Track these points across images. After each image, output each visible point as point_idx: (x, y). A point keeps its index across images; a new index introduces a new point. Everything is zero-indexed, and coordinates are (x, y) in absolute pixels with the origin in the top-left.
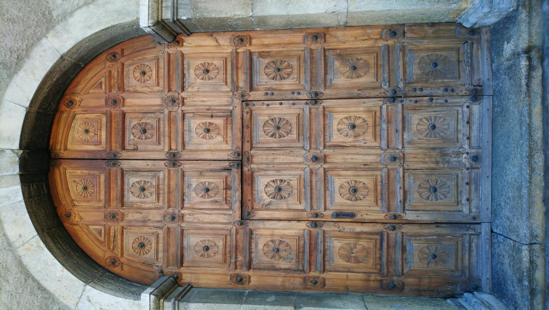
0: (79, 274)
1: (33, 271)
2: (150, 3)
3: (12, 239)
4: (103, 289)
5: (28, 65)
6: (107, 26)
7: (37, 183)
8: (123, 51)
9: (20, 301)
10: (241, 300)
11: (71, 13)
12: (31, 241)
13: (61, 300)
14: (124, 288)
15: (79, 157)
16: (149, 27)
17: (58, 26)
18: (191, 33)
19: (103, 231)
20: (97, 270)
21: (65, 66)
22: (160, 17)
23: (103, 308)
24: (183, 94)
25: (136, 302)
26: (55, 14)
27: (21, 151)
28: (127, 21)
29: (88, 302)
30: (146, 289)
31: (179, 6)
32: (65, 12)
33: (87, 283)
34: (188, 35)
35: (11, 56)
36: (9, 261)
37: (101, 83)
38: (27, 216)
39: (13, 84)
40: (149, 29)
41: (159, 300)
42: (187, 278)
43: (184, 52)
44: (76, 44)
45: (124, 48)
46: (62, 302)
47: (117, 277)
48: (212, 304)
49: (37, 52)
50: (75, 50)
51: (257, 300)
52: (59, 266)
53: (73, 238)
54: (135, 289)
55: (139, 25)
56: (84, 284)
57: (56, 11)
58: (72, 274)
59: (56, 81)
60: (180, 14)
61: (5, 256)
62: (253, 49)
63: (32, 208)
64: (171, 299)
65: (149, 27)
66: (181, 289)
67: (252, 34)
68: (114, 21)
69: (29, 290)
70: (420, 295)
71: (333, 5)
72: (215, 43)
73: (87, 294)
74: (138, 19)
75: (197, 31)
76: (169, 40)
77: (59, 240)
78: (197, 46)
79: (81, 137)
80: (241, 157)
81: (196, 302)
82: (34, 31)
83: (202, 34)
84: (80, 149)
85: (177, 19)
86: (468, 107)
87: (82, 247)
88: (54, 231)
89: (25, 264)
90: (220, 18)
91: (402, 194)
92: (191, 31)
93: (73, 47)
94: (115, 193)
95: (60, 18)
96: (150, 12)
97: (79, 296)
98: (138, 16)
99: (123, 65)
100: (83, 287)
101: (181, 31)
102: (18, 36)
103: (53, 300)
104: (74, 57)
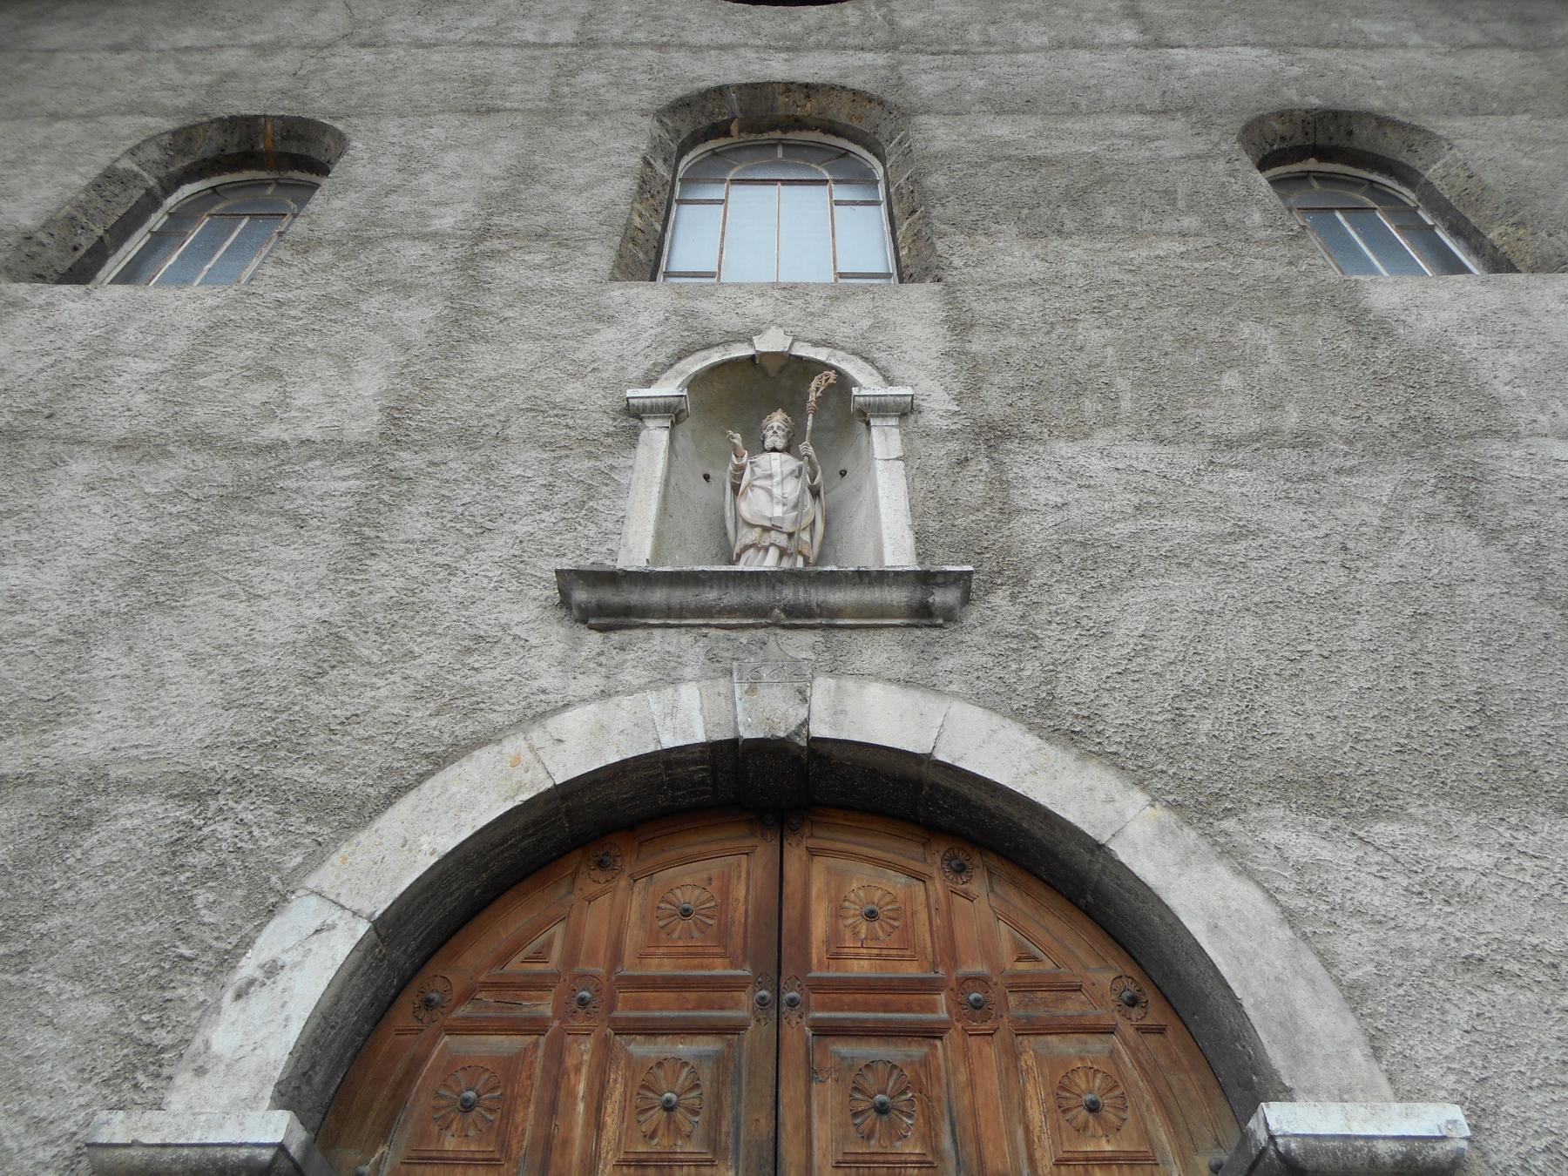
1: (451, 772)
2: (1359, 1143)
3: (553, 724)
4: (344, 974)
5: (1059, 757)
6: (1233, 985)
7: (709, 781)
8: (1161, 1031)
9: (374, 743)
11: (1245, 872)
12: (540, 767)
13: (345, 849)
14: (333, 1041)
15: (787, 889)
17: (1194, 834)
19: (539, 967)
20: (418, 949)
21: (1072, 854)
25: (269, 1091)
26: (1230, 824)
27: (803, 743)
28: (1270, 1053)
29: (317, 924)
32: (1243, 855)
35: (1077, 716)
36: (492, 716)
37: (1035, 959)
38: (614, 758)
39: (996, 720)
40: (1262, 1136)
45: (1170, 1033)
46: (337, 849)
49: (1101, 779)
52: (449, 841)
54: (318, 1079)
56: (377, 915)
57: (1240, 827)
61: (508, 707)
63: (637, 769)
68: (1256, 1006)
69: (396, 765)
74: (1286, 1094)
82: (1162, 772)
89: (476, 753)
94: (664, 1008)
95: (1222, 840)
96: (1331, 1144)
97: (342, 901)
98: (1298, 1093)
99: (1110, 1031)
102: (1136, 734)
103: (350, 826)
104: (1106, 880)
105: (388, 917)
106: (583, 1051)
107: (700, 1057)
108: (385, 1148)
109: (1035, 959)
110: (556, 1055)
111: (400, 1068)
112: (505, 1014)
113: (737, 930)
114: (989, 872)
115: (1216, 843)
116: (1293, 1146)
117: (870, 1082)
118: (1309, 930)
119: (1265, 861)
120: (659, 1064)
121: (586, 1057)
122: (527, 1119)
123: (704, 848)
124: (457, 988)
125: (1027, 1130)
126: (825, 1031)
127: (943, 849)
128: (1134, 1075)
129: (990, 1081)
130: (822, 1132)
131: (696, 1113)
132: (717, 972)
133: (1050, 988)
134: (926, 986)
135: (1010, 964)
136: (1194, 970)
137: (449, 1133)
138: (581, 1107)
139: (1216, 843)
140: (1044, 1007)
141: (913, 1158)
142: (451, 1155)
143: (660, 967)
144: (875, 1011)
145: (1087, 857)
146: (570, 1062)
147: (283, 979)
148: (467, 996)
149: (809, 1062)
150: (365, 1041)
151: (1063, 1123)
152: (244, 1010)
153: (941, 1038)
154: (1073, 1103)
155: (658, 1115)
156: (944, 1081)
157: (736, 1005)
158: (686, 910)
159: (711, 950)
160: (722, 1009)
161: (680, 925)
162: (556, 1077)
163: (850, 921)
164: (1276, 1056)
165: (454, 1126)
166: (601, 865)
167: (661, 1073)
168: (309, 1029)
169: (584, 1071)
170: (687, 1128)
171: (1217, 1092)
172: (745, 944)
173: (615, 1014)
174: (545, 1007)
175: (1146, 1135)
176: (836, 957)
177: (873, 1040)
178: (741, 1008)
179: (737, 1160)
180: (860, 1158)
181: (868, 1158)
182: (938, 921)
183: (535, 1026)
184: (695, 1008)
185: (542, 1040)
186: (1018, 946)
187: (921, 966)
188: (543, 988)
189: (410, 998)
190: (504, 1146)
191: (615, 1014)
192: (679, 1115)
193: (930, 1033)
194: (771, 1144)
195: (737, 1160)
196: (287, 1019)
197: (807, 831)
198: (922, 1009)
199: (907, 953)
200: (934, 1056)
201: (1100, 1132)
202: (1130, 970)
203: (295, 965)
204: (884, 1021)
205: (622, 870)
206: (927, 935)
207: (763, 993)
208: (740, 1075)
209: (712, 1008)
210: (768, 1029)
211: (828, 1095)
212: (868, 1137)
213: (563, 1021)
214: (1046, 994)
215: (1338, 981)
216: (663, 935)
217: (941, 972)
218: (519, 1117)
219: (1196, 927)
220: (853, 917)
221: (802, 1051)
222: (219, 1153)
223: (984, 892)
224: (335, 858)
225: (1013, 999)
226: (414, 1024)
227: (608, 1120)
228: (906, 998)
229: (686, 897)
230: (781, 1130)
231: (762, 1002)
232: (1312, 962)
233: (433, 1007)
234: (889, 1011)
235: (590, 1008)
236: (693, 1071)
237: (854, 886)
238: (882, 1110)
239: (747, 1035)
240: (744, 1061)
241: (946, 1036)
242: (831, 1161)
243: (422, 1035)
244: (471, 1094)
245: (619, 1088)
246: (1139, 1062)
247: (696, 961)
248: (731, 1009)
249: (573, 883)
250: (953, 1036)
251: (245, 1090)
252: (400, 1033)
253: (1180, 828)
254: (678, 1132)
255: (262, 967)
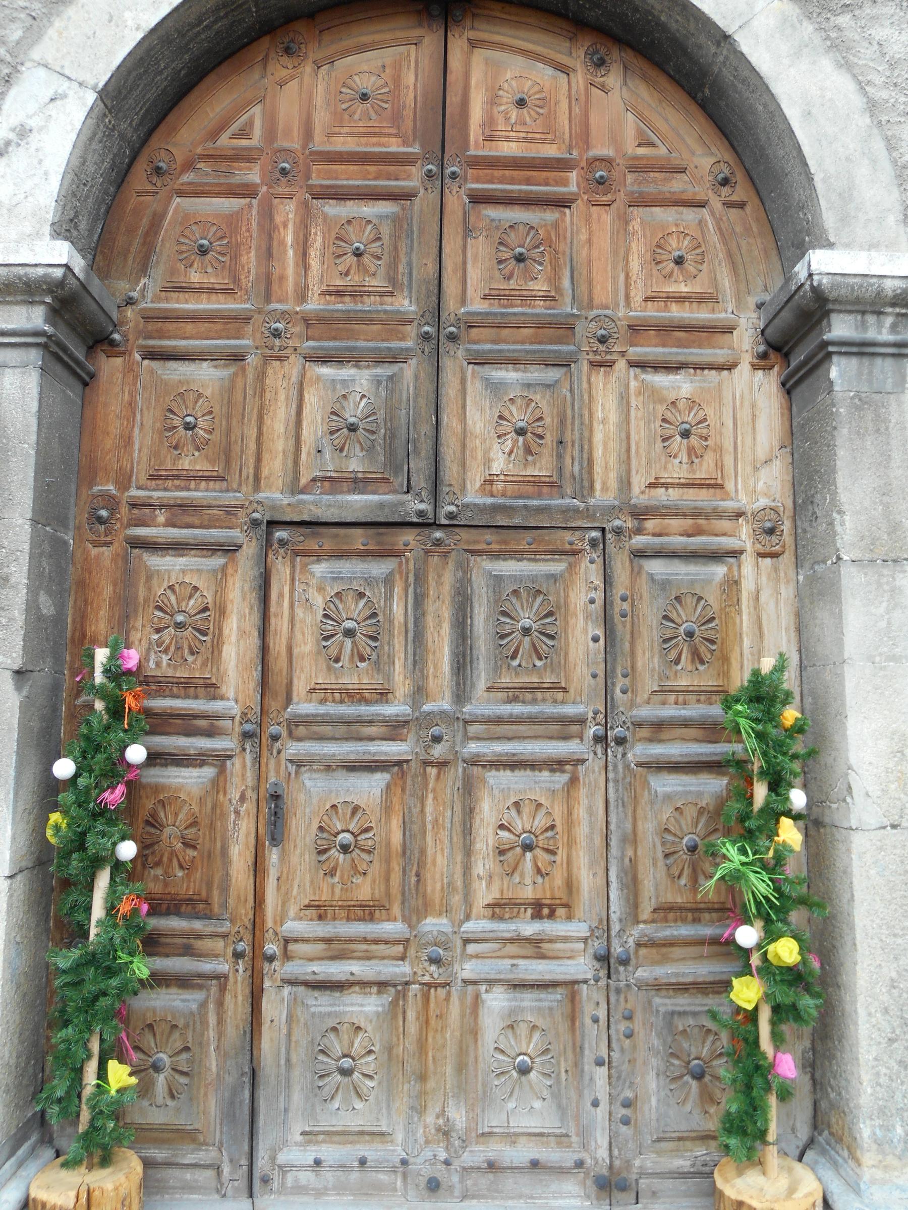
0: (129, 72)
4: (83, 138)
6: (811, 162)
8: (741, 205)
10: (43, 521)
11: (846, 65)
13: (58, 23)
14: (87, 197)
16: (810, 275)
17: (810, 28)
18: (789, 392)
19: (244, 143)
20: (140, 124)
21: (700, 47)
22: (837, 307)
23: (32, 135)
24: (621, 364)
25: (47, 229)
26: (844, 20)
29: (50, 94)
30: (84, 257)
31: (866, 361)
32: (849, 49)
33: (103, 94)
34: (783, 384)
37: (653, 145)
40: (803, 275)
41: (50, 292)
42: (110, 368)
43: (736, 371)
44: (761, 78)
45: (748, 209)
46: (51, 23)
47: (120, 176)
48: (33, 438)
50: (746, 73)
51: (44, 564)
53: (226, 63)
54: (83, 225)
55: (814, 248)
56: (101, 85)
57: (853, 23)
58: (130, 54)
59: (659, 24)
60: (844, 361)
62: (748, 563)
64: (53, 325)
65: (810, 275)
66: (80, 355)
67: (787, 558)
70: (619, 218)
71: (870, 789)
72: (761, 455)
73: (71, 93)
74: (830, 245)
75: (794, 408)
76: (768, 331)
77: (225, 22)
78: (753, 406)
79: (506, 86)
80: (444, 521)
81: (41, 394)
83: (787, 424)
84: (473, 82)
85: (829, 355)
86: (580, 1164)
87: (203, 86)
88: (249, 10)
90: (834, 471)
91: (337, 978)
92: (796, 393)
93: (753, 69)
94: (350, 177)
95: (833, 35)
96: (852, 280)
97: (67, 72)
99: (702, 205)
100: (92, 82)
101: (793, 364)
105: (110, 88)
106: (287, 212)
107: (380, 217)
108: (146, 280)
109: (653, 145)
110: (267, 214)
111: (145, 222)
112: (222, 181)
113: (408, 113)
114: (625, 67)
115: (828, 38)
116: (824, 281)
117: (512, 238)
118: (884, 118)
119: (865, 54)
120: (349, 222)
121: (291, 216)
122: (250, 260)
123: (377, 37)
124: (180, 159)
125: (627, 276)
126: (479, 199)
127: (587, 43)
128: (714, 238)
129: (604, 242)
130: (474, 274)
131: (379, 258)
132: (393, 149)
133: (662, 169)
134: (561, 165)
135: (632, 149)
136: (781, 153)
137: (192, 270)
138: (291, 253)
139: (828, 38)
140: (657, 185)
141: (542, 293)
142: (197, 286)
143: (345, 144)
144: (520, 184)
145: (713, 49)
146: (278, 219)
147: (34, 138)
148: (189, 165)
149: (465, 222)
150: (113, 200)
151: (655, 272)
152: (8, 165)
153: (569, 207)
154: (665, 257)
155: (350, 259)
156: (569, 241)
157: (409, 177)
158: (364, 95)
159: (386, 131)
160: (397, 179)
161: (360, 108)
162: (269, 229)
163: (503, 108)
164: (829, 219)
165: (195, 265)
166: (288, 51)
167: (350, 229)
168: (66, 183)
169: (290, 226)
170: (372, 269)
171: (775, 252)
172: (415, 97)
173: (310, 182)
174: (254, 175)
175: (714, 282)
176: (490, 139)
177: (516, 207)
178: (413, 178)
179: (411, 292)
180: (502, 293)
181: (507, 292)
182: (576, 110)
183: (247, 191)
184: (375, 179)
185: (255, 202)
186: (640, 133)
187: (559, 149)
188: (250, 160)
189: (141, 168)
190: (236, 280)
191: (310, 182)
192: (366, 259)
193: (562, 203)
194: (436, 282)
195: (411, 292)
196: (46, 173)
197: (468, 23)
198: (557, 183)
199: (549, 137)
200: (563, 221)
201: (681, 279)
202: (728, 156)
203: (40, 129)
204: (526, 192)
205: (306, 57)
206: (567, 122)
207: (430, 167)
208: (412, 232)
209: (389, 179)
210: (434, 196)
211: (480, 250)
212: (509, 278)
213: (270, 187)
214: (657, 175)
215: (895, 162)
216: (346, 117)
217: (575, 153)
218: (244, 259)
219: (793, 113)
220: (506, 104)
221: (460, 214)
222: (21, 271)
223: (618, 85)
224: (51, 32)
225: (630, 178)
226: (150, 188)
227: (312, 263)
228: (544, 174)
229: (365, 83)
230: (443, 391)
231: (429, 175)
232: (878, 146)
233: (163, 174)
234: (532, 185)
235: (290, 177)
236: (376, 227)
237: (508, 76)
238: (520, 259)
239: (417, 201)
240: (414, 222)
241: (573, 206)
242: (480, 294)
243: (158, 196)
244: (205, 242)
245: (319, 240)
246: (720, 229)
247: (374, 140)
248: (404, 179)
249: (265, 68)
250: (579, 206)
251: (28, 228)
252: (139, 194)
253: (800, 22)
254: (366, 271)
255: (13, 130)
